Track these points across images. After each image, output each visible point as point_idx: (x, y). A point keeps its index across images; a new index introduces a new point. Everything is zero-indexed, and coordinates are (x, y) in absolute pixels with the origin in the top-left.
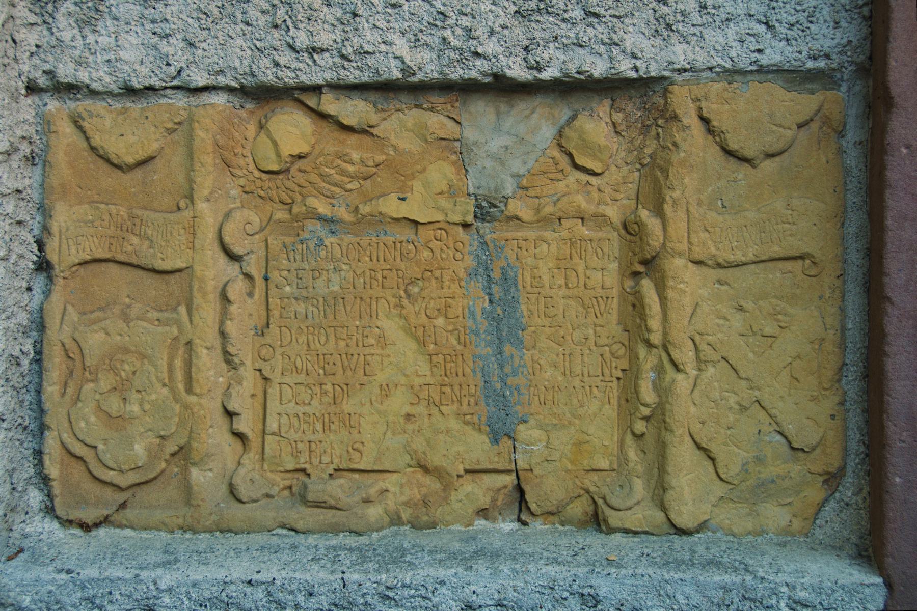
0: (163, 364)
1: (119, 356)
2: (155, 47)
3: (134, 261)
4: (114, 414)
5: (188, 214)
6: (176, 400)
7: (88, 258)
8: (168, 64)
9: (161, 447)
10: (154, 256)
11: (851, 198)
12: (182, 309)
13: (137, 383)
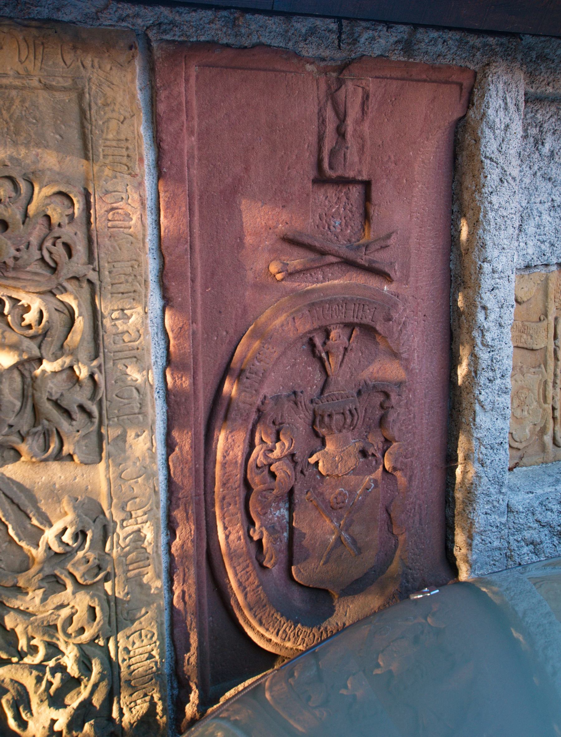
0: (536, 392)
1: (521, 391)
2: (540, 247)
3: (525, 346)
4: (519, 417)
5: (545, 323)
6: (541, 408)
7: (165, 146)
8: (544, 255)
9: (534, 429)
10: (533, 343)
11: (90, 136)
12: (542, 366)
13: (527, 401)
